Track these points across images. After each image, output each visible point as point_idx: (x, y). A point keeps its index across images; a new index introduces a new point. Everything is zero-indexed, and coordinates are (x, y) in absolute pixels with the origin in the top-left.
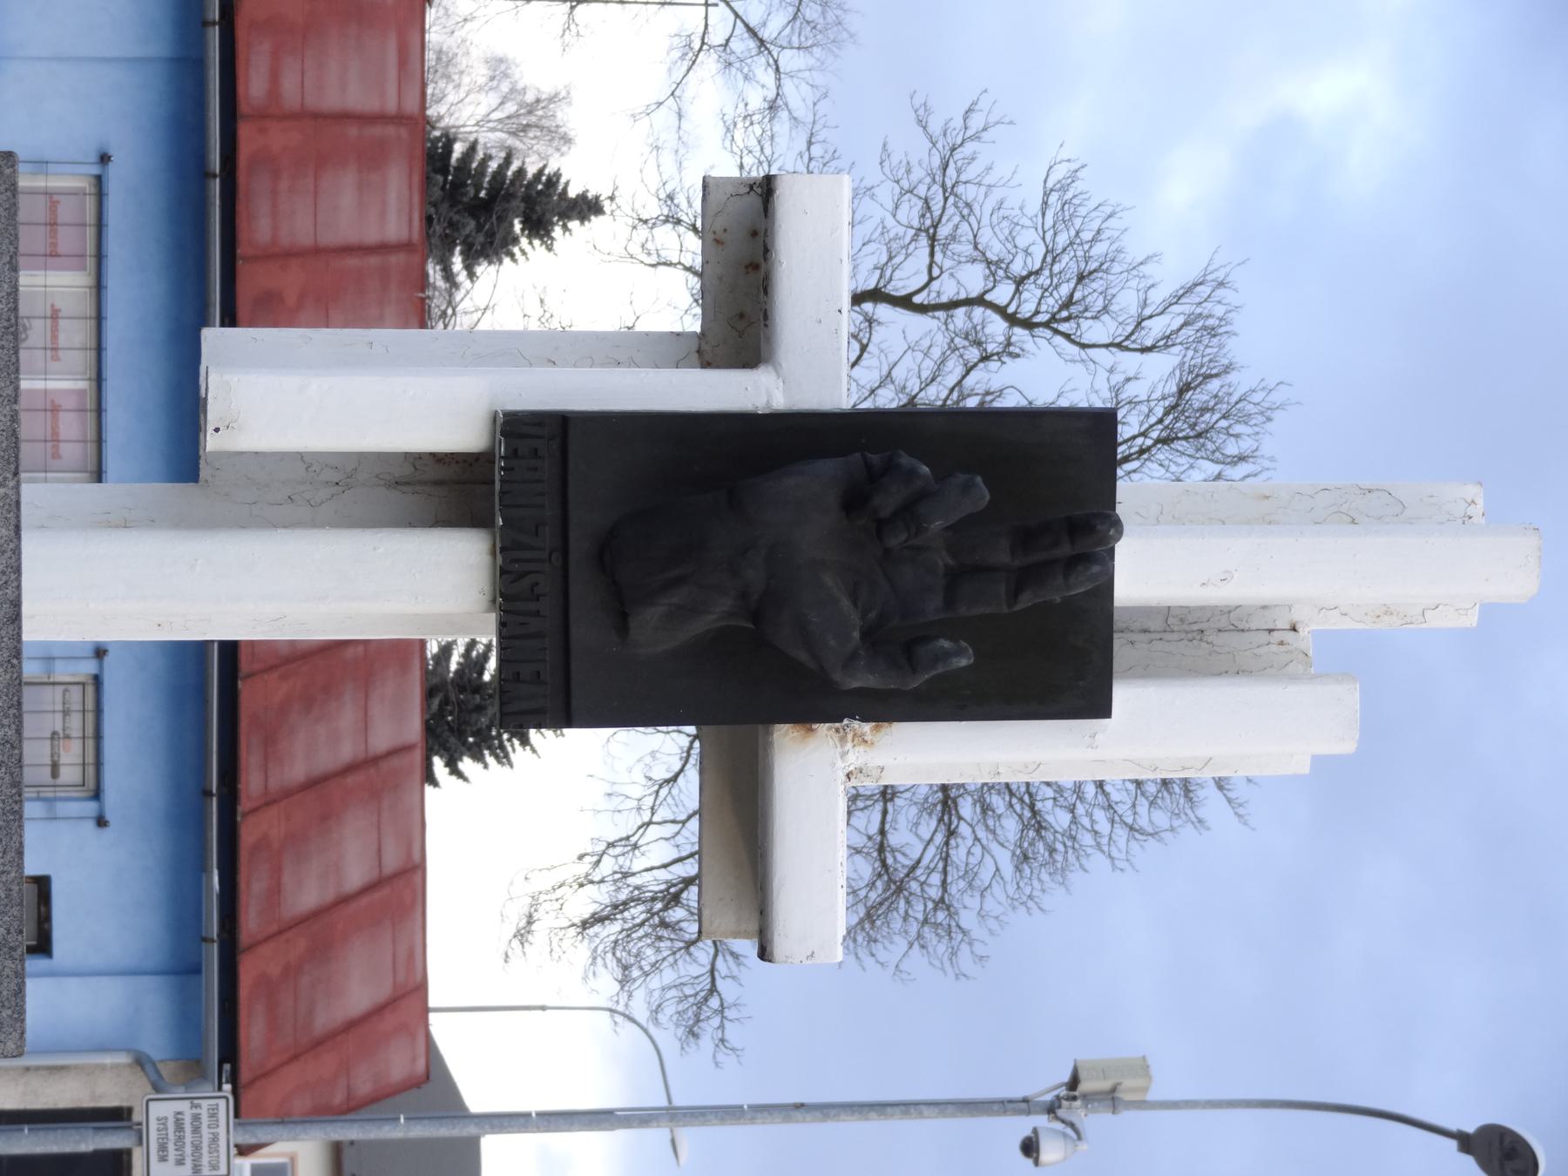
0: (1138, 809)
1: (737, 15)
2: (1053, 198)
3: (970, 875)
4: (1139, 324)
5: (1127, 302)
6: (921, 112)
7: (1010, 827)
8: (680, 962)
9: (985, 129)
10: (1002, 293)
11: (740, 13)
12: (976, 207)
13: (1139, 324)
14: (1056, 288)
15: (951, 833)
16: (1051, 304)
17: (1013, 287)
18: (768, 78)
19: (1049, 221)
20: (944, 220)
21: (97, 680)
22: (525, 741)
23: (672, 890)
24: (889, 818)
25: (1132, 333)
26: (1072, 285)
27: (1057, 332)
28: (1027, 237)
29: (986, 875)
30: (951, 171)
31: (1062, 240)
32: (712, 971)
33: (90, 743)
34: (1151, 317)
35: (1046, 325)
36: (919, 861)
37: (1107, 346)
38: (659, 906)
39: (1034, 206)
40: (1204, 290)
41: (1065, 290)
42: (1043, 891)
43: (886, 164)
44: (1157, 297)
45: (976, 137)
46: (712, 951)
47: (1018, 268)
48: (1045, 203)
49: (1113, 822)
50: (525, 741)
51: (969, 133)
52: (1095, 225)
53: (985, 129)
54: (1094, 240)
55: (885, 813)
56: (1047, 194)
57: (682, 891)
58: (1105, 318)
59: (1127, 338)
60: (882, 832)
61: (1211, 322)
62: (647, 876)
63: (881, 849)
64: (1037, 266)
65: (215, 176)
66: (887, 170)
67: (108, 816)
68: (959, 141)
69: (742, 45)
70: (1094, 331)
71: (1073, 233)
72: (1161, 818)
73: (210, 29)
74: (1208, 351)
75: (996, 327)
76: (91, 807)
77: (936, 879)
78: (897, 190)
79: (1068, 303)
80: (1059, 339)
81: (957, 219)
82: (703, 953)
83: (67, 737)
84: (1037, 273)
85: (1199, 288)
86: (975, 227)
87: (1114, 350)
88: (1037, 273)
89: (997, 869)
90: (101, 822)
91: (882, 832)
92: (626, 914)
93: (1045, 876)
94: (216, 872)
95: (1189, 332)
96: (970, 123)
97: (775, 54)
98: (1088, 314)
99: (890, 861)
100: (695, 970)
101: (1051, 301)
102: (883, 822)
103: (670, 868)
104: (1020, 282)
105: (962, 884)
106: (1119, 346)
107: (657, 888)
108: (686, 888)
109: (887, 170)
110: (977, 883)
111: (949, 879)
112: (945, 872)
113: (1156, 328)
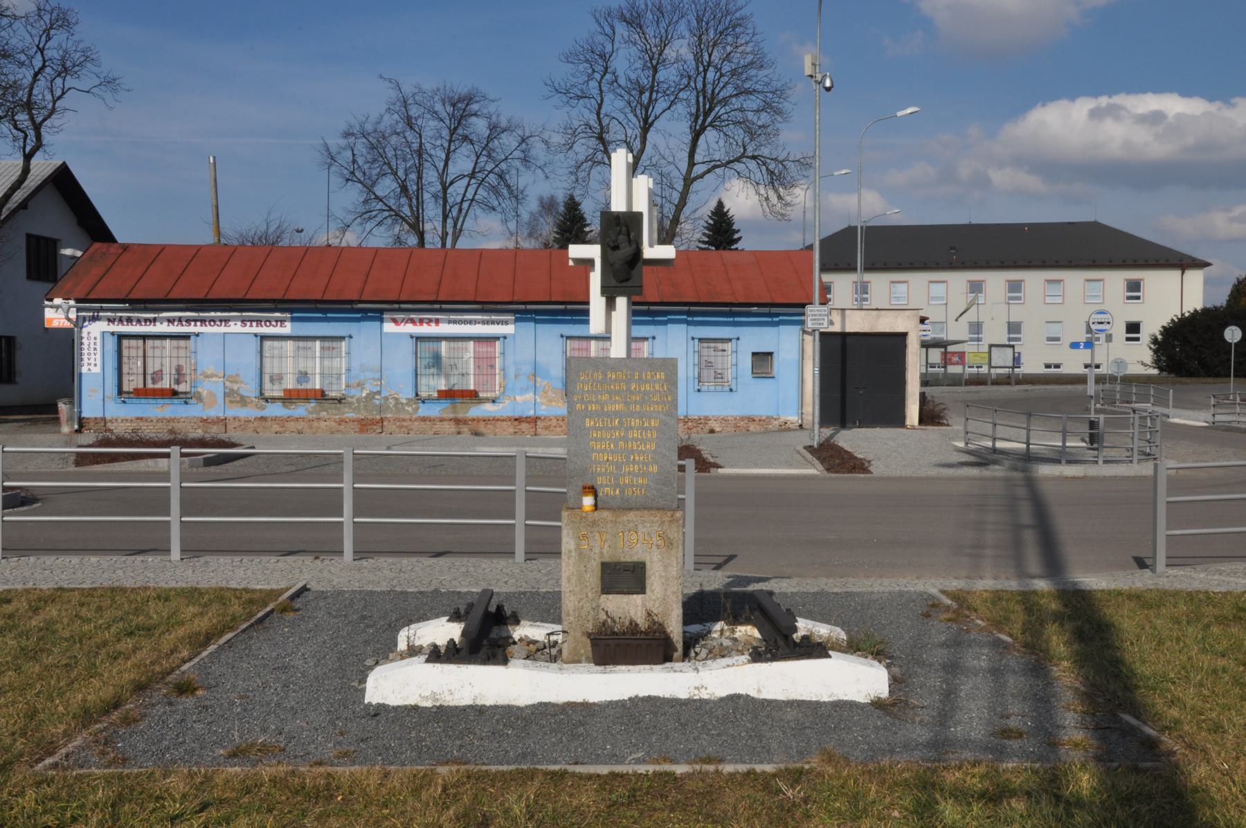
3: (767, 84)
5: (601, 38)
7: (753, 72)
10: (597, 76)
21: (700, 340)
28: (581, 68)
44: (599, 29)
47: (590, 71)
69: (524, 145)
70: (609, 48)
72: (750, 25)
75: (608, 76)
104: (594, 71)
113: (608, 30)
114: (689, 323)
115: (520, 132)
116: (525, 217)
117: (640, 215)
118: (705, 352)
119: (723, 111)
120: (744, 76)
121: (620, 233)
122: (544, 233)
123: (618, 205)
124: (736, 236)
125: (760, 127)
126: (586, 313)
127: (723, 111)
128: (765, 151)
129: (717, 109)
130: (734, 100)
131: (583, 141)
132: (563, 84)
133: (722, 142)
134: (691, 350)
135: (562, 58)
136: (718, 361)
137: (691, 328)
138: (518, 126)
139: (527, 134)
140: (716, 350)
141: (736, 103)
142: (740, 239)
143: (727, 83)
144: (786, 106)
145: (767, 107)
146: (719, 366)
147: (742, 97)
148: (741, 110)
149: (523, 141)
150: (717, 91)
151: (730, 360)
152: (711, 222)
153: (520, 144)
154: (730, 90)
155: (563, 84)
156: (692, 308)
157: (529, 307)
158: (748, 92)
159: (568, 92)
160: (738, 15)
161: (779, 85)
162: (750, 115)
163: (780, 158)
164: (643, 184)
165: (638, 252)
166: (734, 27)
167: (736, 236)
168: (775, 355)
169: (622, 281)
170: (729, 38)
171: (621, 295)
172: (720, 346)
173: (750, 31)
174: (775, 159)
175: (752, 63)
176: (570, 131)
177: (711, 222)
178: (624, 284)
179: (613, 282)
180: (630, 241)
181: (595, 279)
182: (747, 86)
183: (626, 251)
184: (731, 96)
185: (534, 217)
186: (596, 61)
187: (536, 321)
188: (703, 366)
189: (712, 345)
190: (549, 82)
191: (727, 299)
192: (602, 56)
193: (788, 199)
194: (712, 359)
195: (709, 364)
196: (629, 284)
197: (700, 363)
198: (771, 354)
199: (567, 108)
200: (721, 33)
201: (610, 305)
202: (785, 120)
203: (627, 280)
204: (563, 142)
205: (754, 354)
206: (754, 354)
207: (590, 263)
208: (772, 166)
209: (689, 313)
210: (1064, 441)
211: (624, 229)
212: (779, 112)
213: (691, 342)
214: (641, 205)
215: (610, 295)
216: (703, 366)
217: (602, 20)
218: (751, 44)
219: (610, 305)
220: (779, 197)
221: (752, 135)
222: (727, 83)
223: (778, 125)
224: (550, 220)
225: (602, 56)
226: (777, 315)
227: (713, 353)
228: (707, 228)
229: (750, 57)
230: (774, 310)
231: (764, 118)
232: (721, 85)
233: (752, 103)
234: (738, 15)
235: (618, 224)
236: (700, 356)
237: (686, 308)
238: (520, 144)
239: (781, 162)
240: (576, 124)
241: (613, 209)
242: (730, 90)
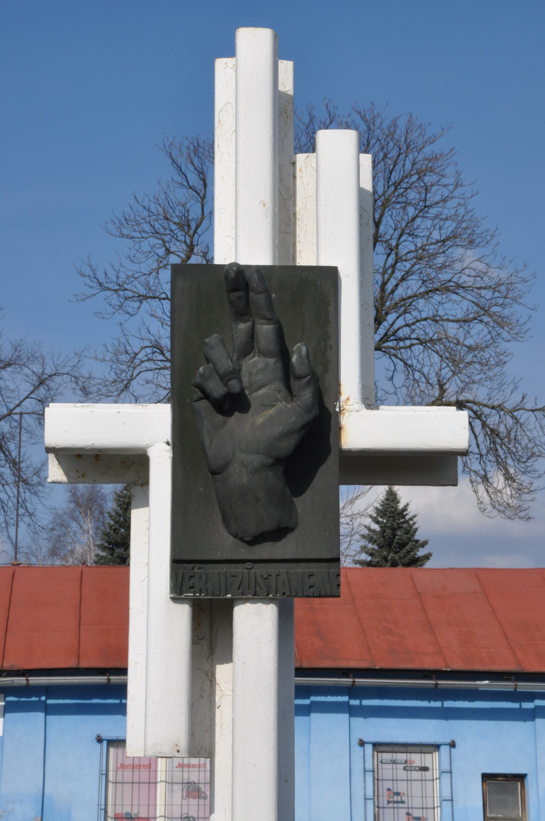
0: (446, 183)
1: (27, 397)
2: (125, 232)
3: (480, 275)
4: (191, 187)
6: (79, 298)
7: (458, 252)
8: (529, 427)
9: (91, 266)
11: (27, 393)
12: (130, 274)
13: (191, 187)
14: (172, 231)
15: (458, 286)
16: (180, 235)
17: (171, 255)
18: (57, 379)
19: (137, 235)
20: (135, 290)
21: (376, 746)
22: (405, 509)
23: (489, 433)
24: (451, 318)
25: (196, 192)
26: (171, 223)
27: (195, 232)
28: (145, 246)
29: (480, 266)
30: (110, 286)
31: (147, 228)
32: (533, 411)
33: (409, 749)
34: (188, 182)
35: (192, 237)
36: (473, 302)
37: (203, 206)
38: (498, 440)
39: (130, 242)
40: (175, 152)
41: (173, 227)
42: (488, 231)
43: (105, 316)
44: (179, 179)
45: (94, 271)
46: (521, 411)
47: (162, 252)
48: (127, 237)
49: (453, 197)
50: (405, 509)
51: (92, 275)
52: (141, 209)
53: (91, 266)
54: (149, 210)
55: (448, 320)
56: (123, 236)
57: (489, 428)
58: (188, 206)
59: (199, 194)
60: (458, 321)
61: (192, 148)
62: (482, 446)
63: (465, 321)
64: (160, 242)
65: (109, 680)
66: (108, 316)
67: (449, 741)
68: (96, 280)
69: (42, 391)
71: (143, 221)
72: (450, 171)
73: (31, 682)
74: (206, 149)
76: (444, 749)
77: (483, 292)
78: (120, 311)
79: (181, 226)
80: (199, 231)
81: (136, 283)
82: (523, 416)
83: (406, 762)
84: (164, 241)
85: (173, 155)
86: (139, 274)
87: (205, 202)
88: (164, 241)
89: (477, 260)
90: (453, 745)
91: (458, 321)
92: (503, 457)
93: (479, 231)
94: (478, 683)
95: (196, 161)
96: (87, 274)
97: (46, 376)
98: (186, 215)
99: (471, 316)
100: (532, 419)
101: (179, 234)
102: (453, 321)
103: (477, 434)
104: (168, 252)
105: (485, 278)
106: (203, 199)
107: (489, 441)
108: (488, 426)
109: (108, 316)
110: (484, 270)
111: (484, 285)
112: (479, 288)
114: (353, 712)
115: (37, 368)
116: (45, 518)
117: (331, 275)
118: (387, 771)
119: (400, 322)
120: (440, 260)
121: (249, 346)
122: (79, 549)
123: (239, 239)
124: (421, 552)
125: (470, 348)
126: (121, 691)
127: (400, 322)
128: (480, 393)
129: (391, 318)
130: (421, 302)
131: (149, 375)
132: (112, 275)
133: (400, 378)
134: (358, 767)
135: (111, 228)
136: (414, 792)
137: (358, 721)
138: (32, 358)
139: (49, 370)
140: (408, 767)
141: (424, 307)
142: (427, 557)
143: (408, 273)
144: (516, 311)
145: (483, 312)
146: (417, 802)
147: (437, 297)
148: (435, 319)
149: (42, 382)
150: (389, 287)
151: (438, 789)
152: (376, 527)
153: (36, 388)
154: (414, 285)
155: (112, 275)
156: (360, 681)
157: (35, 680)
158: (445, 289)
159: (121, 288)
160: (428, 151)
161: (503, 275)
162: (452, 329)
163: (509, 405)
164: (338, 166)
165: (322, 423)
166: (421, 174)
167: (421, 552)
168: (530, 781)
169: (256, 540)
170: (412, 195)
171: (256, 594)
172: (417, 759)
173: (450, 180)
174: (499, 408)
175: (454, 236)
176: (124, 358)
177: (376, 527)
178: (265, 551)
179: (224, 543)
180: (287, 373)
181: (152, 530)
182: (444, 276)
183: (270, 418)
184: (415, 296)
185: (60, 523)
186: (174, 236)
187: (48, 710)
188: (383, 802)
189: (401, 757)
190: (87, 271)
191: (429, 664)
192: (185, 225)
193: (525, 479)
194: (401, 787)
195: (396, 798)
196: (285, 548)
197: (376, 795)
198: (521, 778)
199: (120, 317)
200: (397, 185)
201: (211, 635)
202: (517, 336)
203: (278, 533)
204: (112, 377)
205: (486, 777)
206: (486, 777)
207: (130, 465)
208: (493, 420)
209: (353, 691)
210: (109, 680)
211: (265, 330)
212: (501, 322)
213: (358, 750)
214: (331, 240)
215: (208, 599)
216: (383, 802)
217: (182, 161)
218: (452, 204)
219: (211, 635)
220: (508, 477)
221: (456, 364)
222: (408, 273)
223: (503, 346)
224: (89, 525)
225: (185, 225)
226: (531, 696)
227: (402, 774)
228: (371, 540)
229: (450, 227)
230: (524, 686)
231: (478, 333)
232: (398, 275)
233: (456, 306)
234: (428, 151)
235: (243, 312)
236: (377, 780)
237: (347, 681)
238: (36, 388)
239: (511, 412)
240: (135, 345)
241: (223, 255)
242: (414, 285)
